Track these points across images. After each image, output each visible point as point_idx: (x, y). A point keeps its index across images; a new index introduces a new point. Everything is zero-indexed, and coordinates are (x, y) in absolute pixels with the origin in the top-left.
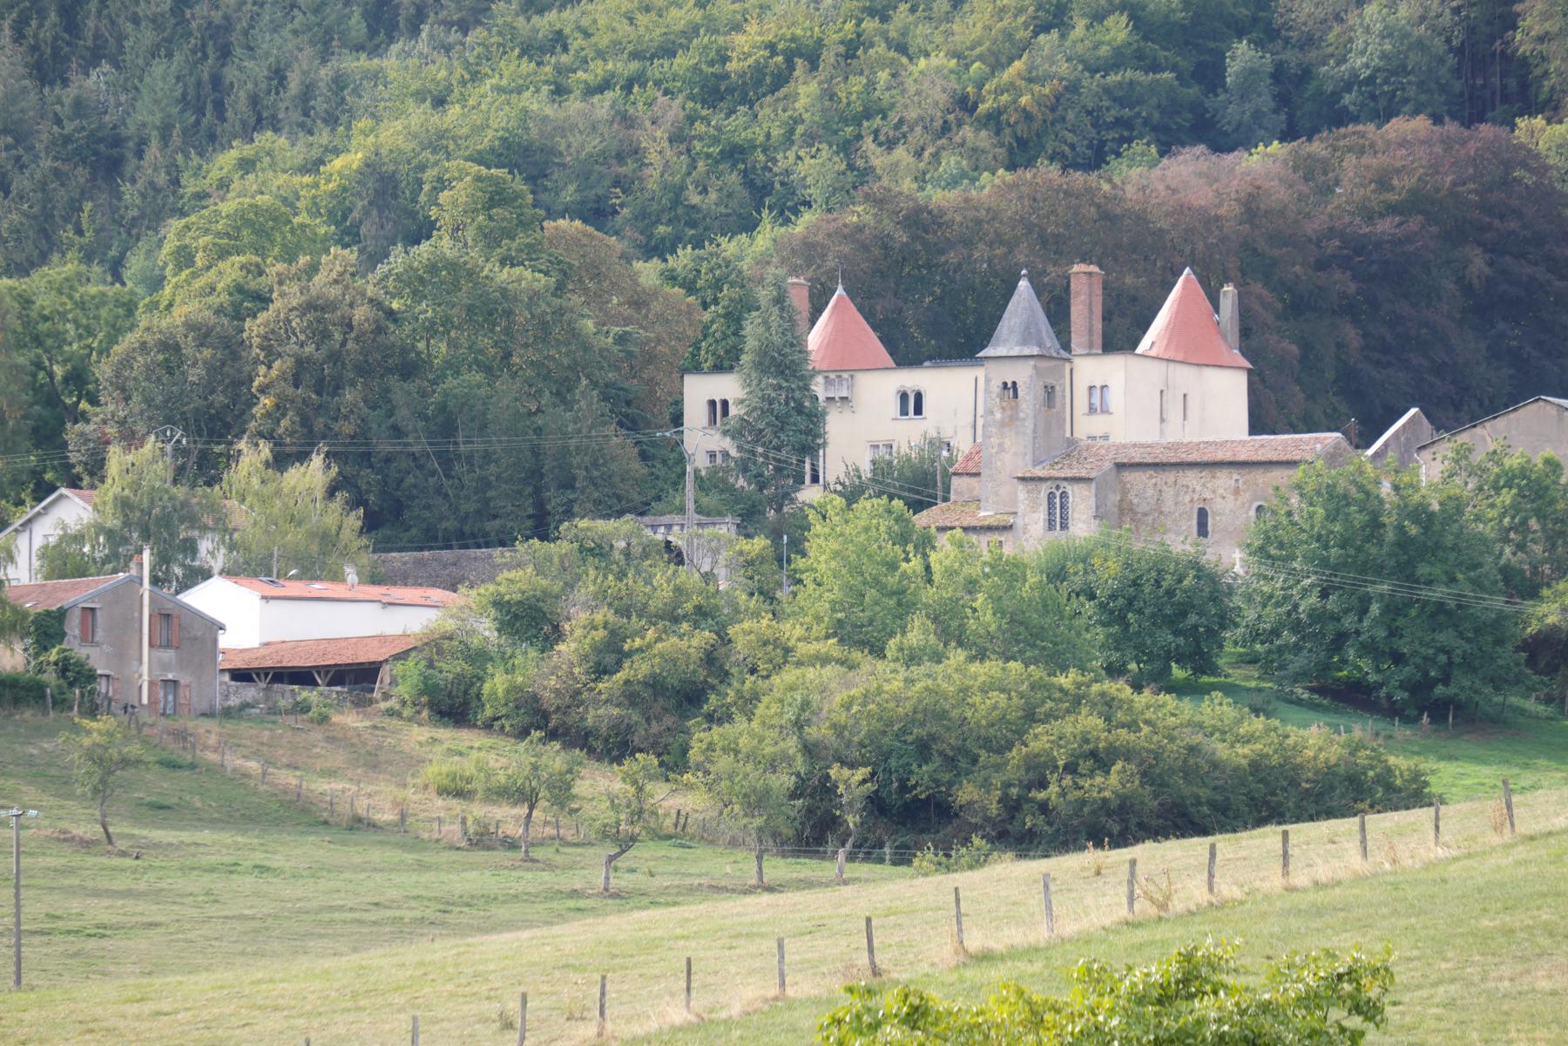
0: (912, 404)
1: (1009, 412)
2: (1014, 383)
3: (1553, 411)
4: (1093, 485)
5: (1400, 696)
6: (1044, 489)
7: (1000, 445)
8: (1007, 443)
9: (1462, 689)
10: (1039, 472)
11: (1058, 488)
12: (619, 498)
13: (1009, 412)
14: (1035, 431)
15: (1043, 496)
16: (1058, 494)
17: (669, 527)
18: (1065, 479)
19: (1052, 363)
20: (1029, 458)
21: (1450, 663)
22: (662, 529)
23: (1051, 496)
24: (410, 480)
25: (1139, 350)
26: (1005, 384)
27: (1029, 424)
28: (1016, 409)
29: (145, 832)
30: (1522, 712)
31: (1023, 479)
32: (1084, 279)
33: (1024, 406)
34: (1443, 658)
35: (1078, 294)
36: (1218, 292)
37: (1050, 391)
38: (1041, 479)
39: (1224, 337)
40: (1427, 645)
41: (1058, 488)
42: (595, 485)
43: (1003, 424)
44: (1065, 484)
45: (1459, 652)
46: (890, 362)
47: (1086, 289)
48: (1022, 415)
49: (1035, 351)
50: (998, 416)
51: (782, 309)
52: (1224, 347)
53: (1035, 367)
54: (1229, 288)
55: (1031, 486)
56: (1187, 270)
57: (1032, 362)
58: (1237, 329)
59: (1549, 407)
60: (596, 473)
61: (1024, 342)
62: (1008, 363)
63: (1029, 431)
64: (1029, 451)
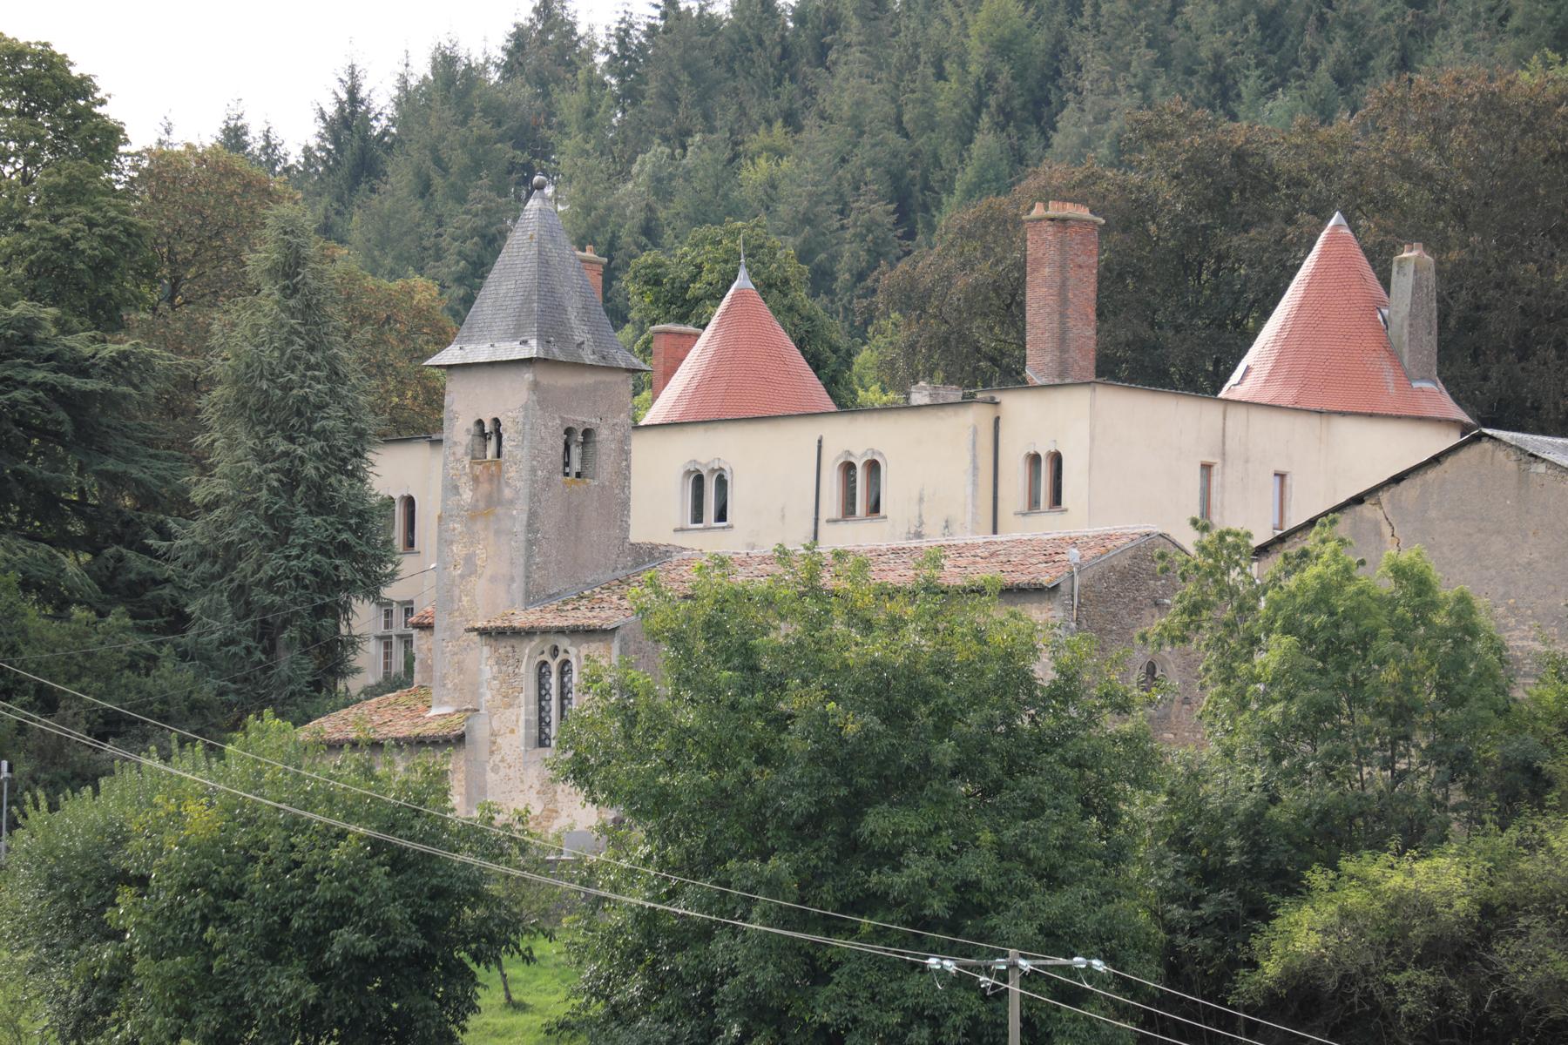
0: (861, 486)
1: (485, 487)
2: (496, 421)
4: (616, 645)
6: (529, 653)
7: (469, 559)
8: (481, 553)
10: (521, 620)
11: (555, 651)
13: (485, 487)
16: (554, 665)
18: (561, 631)
19: (589, 379)
20: (518, 586)
23: (542, 670)
26: (480, 423)
27: (520, 513)
28: (496, 478)
31: (484, 632)
32: (1049, 231)
35: (1039, 263)
37: (578, 440)
38: (529, 633)
39: (1394, 355)
43: (474, 514)
44: (564, 643)
46: (833, 408)
47: (1053, 254)
48: (508, 493)
49: (532, 349)
50: (467, 495)
52: (1389, 376)
53: (535, 386)
54: (1411, 254)
55: (504, 648)
56: (1337, 218)
57: (528, 376)
58: (1430, 341)
59: (1501, 454)
61: (517, 333)
62: (485, 375)
63: (519, 527)
64: (519, 571)
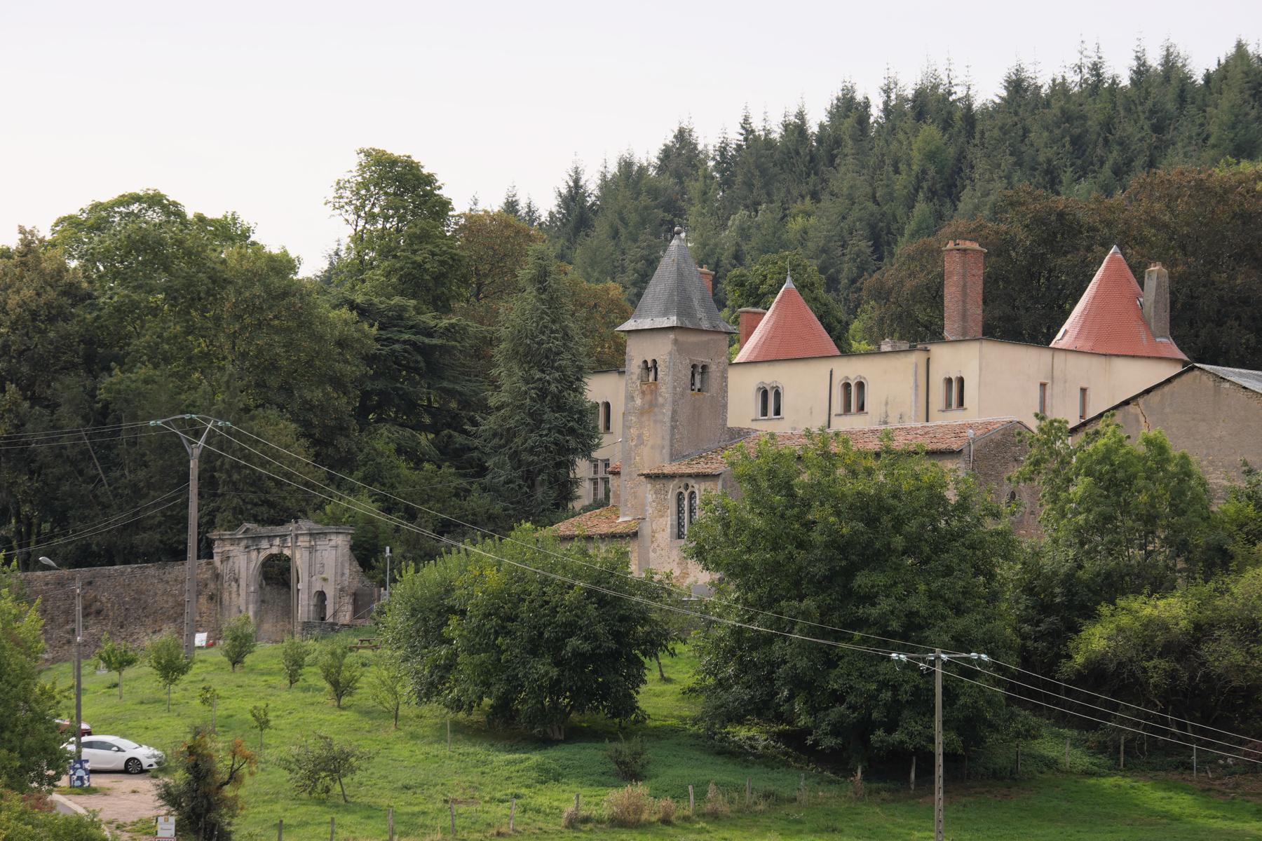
1: (648, 397)
2: (654, 361)
3: (1208, 382)
5: (830, 742)
6: (672, 487)
7: (640, 436)
8: (646, 433)
9: (911, 735)
10: (668, 469)
11: (687, 487)
12: (271, 505)
13: (648, 397)
14: (673, 419)
15: (671, 498)
16: (686, 494)
17: (283, 537)
18: (690, 476)
20: (666, 451)
21: (896, 701)
22: (277, 541)
24: (65, 487)
25: (1060, 341)
27: (667, 410)
28: (655, 392)
29: (1239, 825)
30: (1052, 764)
31: (648, 476)
32: (957, 257)
33: (663, 389)
34: (887, 695)
36: (1143, 272)
38: (672, 477)
39: (1146, 324)
40: (869, 678)
41: (687, 487)
42: (237, 490)
43: (642, 412)
44: (692, 482)
45: (907, 687)
47: (959, 268)
48: (661, 400)
49: (673, 321)
50: (638, 402)
51: (543, 290)
53: (676, 342)
54: (1155, 268)
56: (1114, 249)
57: (672, 336)
58: (1166, 316)
59: (1204, 378)
60: (236, 477)
63: (667, 419)
64: (667, 443)
